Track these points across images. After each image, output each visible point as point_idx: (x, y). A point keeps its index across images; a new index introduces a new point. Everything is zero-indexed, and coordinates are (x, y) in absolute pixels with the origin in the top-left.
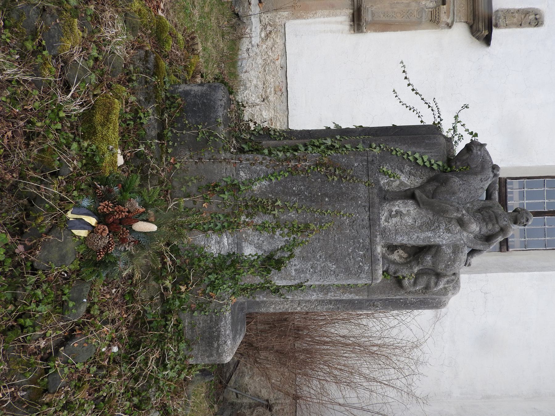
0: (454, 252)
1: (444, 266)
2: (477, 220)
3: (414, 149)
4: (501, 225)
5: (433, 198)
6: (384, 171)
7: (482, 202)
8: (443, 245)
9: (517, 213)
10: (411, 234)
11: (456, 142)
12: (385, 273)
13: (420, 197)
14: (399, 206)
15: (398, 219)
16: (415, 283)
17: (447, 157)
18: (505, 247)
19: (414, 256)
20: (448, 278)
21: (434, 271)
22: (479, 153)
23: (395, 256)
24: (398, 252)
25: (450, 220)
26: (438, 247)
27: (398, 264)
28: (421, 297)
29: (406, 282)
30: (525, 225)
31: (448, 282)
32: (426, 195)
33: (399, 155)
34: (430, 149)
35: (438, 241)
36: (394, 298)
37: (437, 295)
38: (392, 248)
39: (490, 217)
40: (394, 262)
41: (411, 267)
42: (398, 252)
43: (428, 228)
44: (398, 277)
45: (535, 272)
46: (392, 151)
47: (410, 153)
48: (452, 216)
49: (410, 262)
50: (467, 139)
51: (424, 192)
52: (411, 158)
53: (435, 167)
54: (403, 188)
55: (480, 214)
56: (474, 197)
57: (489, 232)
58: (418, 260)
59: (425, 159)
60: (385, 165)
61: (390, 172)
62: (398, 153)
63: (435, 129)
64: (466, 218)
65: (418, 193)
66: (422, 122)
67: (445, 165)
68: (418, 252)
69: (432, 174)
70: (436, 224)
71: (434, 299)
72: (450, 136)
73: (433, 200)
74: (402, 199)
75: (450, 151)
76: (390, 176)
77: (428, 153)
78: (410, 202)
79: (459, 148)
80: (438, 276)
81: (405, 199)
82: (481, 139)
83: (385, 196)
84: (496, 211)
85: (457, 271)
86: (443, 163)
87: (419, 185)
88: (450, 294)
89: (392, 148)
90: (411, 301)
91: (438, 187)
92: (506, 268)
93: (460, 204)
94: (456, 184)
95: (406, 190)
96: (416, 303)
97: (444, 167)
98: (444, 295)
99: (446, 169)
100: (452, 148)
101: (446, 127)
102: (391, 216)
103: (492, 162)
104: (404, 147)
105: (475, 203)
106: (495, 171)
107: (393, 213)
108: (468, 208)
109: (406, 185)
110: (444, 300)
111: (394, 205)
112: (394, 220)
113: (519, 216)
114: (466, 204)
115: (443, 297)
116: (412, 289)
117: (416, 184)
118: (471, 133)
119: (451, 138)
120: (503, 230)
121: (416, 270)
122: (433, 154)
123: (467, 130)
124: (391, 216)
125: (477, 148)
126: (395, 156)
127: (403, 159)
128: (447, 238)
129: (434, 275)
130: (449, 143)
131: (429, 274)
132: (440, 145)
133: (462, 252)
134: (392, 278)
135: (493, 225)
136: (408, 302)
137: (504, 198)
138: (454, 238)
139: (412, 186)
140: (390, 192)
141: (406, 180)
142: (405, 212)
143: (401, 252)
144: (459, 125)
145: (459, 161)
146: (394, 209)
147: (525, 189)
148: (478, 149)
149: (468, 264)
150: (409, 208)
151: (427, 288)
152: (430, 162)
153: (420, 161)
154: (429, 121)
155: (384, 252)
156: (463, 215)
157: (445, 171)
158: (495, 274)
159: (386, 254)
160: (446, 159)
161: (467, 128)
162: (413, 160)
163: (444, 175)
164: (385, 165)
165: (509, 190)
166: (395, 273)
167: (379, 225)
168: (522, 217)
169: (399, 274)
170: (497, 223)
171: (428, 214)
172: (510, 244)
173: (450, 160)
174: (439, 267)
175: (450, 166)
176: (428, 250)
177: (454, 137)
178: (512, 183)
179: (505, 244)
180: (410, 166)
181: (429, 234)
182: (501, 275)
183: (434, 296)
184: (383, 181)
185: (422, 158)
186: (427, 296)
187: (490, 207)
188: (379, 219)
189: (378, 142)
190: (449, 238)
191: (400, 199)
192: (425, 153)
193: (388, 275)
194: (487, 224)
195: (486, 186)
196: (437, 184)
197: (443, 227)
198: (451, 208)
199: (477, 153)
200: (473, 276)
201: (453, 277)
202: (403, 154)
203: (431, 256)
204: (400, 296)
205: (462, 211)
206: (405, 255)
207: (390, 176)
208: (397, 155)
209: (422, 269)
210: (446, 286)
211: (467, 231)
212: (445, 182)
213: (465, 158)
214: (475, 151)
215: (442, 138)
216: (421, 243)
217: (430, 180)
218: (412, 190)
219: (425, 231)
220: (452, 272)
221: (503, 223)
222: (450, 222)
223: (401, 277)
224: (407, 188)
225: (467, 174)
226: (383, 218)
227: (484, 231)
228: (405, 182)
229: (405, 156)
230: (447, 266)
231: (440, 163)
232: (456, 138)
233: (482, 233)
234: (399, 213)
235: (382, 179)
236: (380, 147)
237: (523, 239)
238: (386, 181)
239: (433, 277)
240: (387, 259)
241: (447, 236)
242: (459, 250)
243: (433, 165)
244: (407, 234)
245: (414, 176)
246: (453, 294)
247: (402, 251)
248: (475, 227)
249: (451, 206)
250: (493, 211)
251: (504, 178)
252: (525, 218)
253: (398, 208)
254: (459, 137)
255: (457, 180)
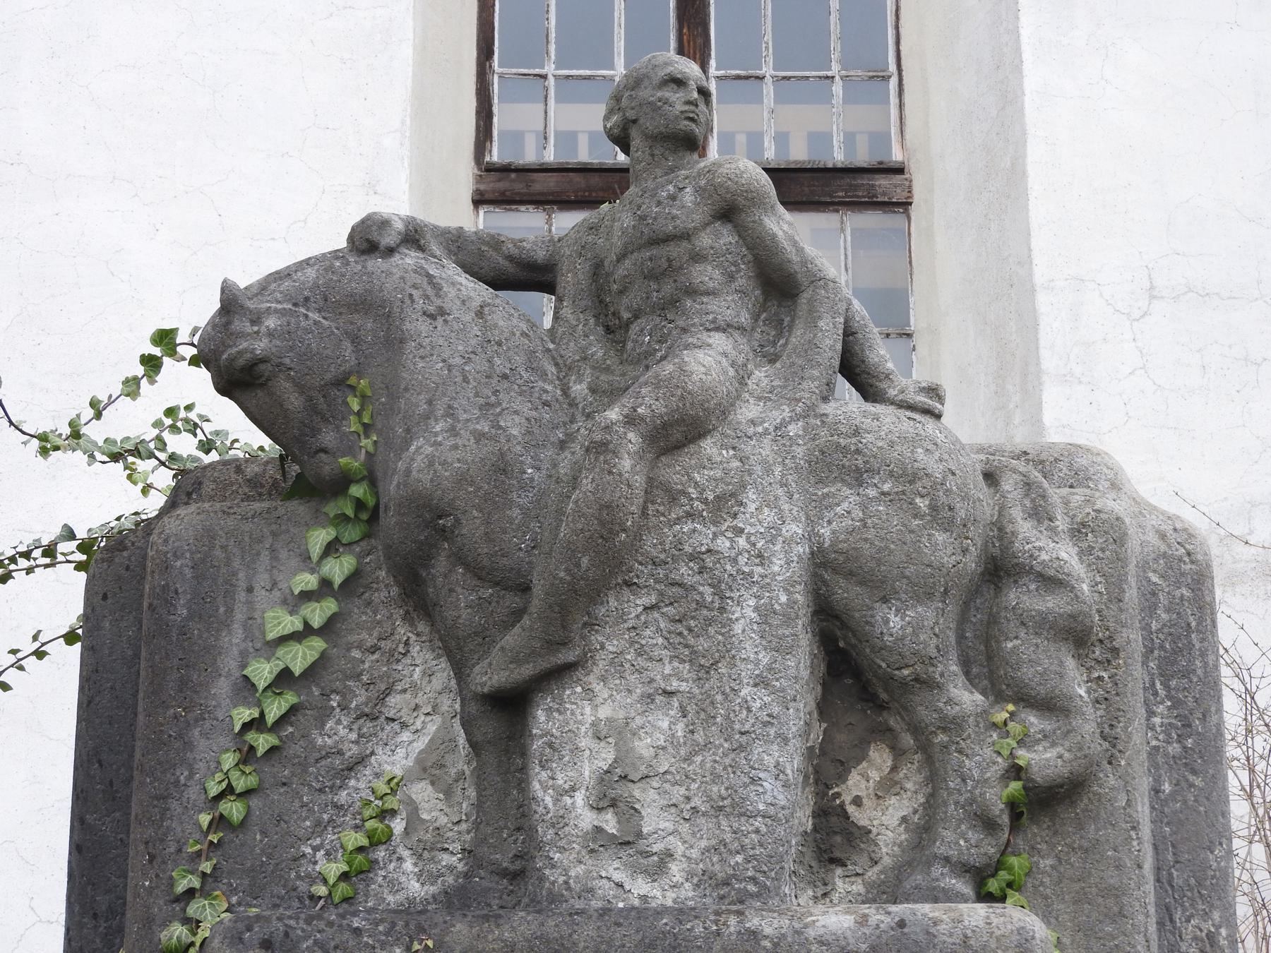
0: (858, 477)
1: (940, 537)
2: (668, 343)
3: (222, 688)
4: (698, 218)
5: (526, 589)
6: (345, 876)
7: (567, 312)
8: (812, 535)
9: (634, 132)
10: (744, 722)
11: (207, 447)
12: (993, 886)
13: (516, 660)
14: (565, 788)
15: (648, 799)
16: (1052, 706)
17: (289, 495)
18: (882, 182)
19: (881, 707)
20: (1016, 513)
21: (972, 594)
22: (271, 322)
23: (886, 819)
24: (857, 801)
25: (660, 493)
26: (825, 567)
27: (932, 805)
28: (1136, 672)
29: (1045, 760)
30: (704, 93)
31: (1040, 514)
32: (507, 625)
33: (252, 781)
34: (229, 594)
35: (785, 568)
36: (1146, 831)
37: (1122, 579)
38: (832, 840)
39: (654, 276)
40: (923, 831)
41: (953, 725)
42: (857, 801)
43: (709, 622)
44: (1012, 805)
45: (1025, 33)
46: (220, 822)
47: (244, 714)
48: (639, 481)
49: (916, 729)
50: (189, 384)
51: (485, 638)
52: (274, 710)
53: (338, 569)
54: (460, 761)
55: (635, 328)
56: (531, 354)
57: (741, 282)
58: (904, 684)
59: (291, 623)
60: (306, 868)
61: (354, 839)
62: (240, 784)
63: (117, 565)
64: (650, 404)
65: (492, 674)
66: (70, 638)
67: (332, 509)
68: (856, 684)
69: (385, 588)
70: (685, 572)
71: (1150, 597)
72: (164, 479)
73: (538, 590)
74: (523, 769)
75: (254, 482)
76: (376, 841)
77: (250, 604)
78: (542, 719)
79: (243, 434)
80: (1000, 569)
81: (524, 753)
82: (194, 313)
83: (504, 874)
84: (618, 242)
85: (975, 463)
86: (319, 520)
87: (444, 663)
88: (1110, 504)
89: (205, 819)
90: (1168, 728)
91: (459, 558)
92: (1004, 180)
93: (570, 437)
94: (452, 456)
95: (469, 741)
96: (1177, 704)
97: (343, 519)
98: (1120, 540)
99: (359, 504)
100: (238, 466)
101: (108, 499)
102: (628, 842)
103: (336, 254)
104: (202, 744)
105: (570, 352)
106: (388, 240)
107: (610, 823)
108: (593, 390)
109: (442, 744)
110: (1152, 538)
111: (559, 822)
112: (655, 821)
113: (649, 124)
114: (573, 404)
115: (1133, 545)
116: (1088, 724)
117: (438, 682)
118: (152, 364)
119: (181, 474)
120: (730, 210)
121: (966, 698)
122: (262, 579)
123: (131, 387)
124: (628, 842)
125: (242, 335)
126: (255, 802)
127: (277, 753)
128: (768, 515)
129: (998, 589)
130: (208, 487)
131: (993, 620)
132: (209, 535)
133: (857, 432)
134: (1020, 842)
135: (697, 257)
136: (1174, 749)
137: (595, 180)
138: (768, 471)
139: (451, 704)
140: (481, 841)
141: (411, 741)
142: (607, 756)
143: (857, 784)
144: (96, 432)
145: (315, 431)
146: (586, 819)
147: (550, 69)
148: (249, 329)
149: (928, 405)
150: (585, 728)
151: (1077, 635)
152: (307, 596)
153: (299, 658)
154: (61, 596)
155: (858, 887)
156: (631, 420)
157: (370, 515)
158: (1040, 242)
159: (872, 874)
160: (298, 508)
161: (117, 389)
162: (290, 698)
163: (389, 520)
164: (306, 868)
165: (550, 156)
166: (989, 825)
167: (681, 913)
168: (655, 108)
169: (996, 798)
170: (686, 236)
171: (622, 617)
172: (863, 158)
173: (303, 479)
174: (948, 561)
175: (341, 484)
176: (844, 626)
177: (173, 457)
178: (516, 138)
179: (863, 180)
180: (324, 714)
181: (744, 613)
182: (1040, 208)
183: (1132, 594)
184: (407, 880)
185: (283, 640)
186: (1132, 639)
187: (597, 269)
188: (643, 913)
189: (160, 906)
190: (773, 504)
191: (522, 784)
192: (253, 626)
193: (999, 865)
194: (692, 292)
195: (478, 291)
196: (441, 564)
197: (702, 535)
198: (586, 483)
199: (271, 334)
200: (1049, 361)
201: (1009, 484)
202: (247, 756)
203: (881, 611)
204: (1132, 792)
205: (608, 428)
206: (879, 759)
207: (376, 841)
208: (248, 793)
209: (966, 664)
210: (1062, 523)
211: (734, 399)
212: (433, 519)
213: (294, 401)
214: (261, 346)
215: (171, 525)
216: (800, 663)
217: (417, 598)
218: (473, 708)
219: (728, 636)
220: (981, 491)
221: (688, 206)
222: (673, 497)
223: (1015, 786)
224: (462, 739)
225: (393, 389)
226: (640, 887)
227: (731, 305)
228: (421, 744)
229: (263, 742)
230: (941, 516)
231: (319, 538)
232: (184, 445)
233: (744, 318)
234: (612, 792)
235: (394, 886)
236: (190, 893)
237: (838, 88)
238: (408, 865)
239: (1012, 596)
240: (901, 870)
241: (755, 514)
242: (845, 450)
243: (326, 583)
244: (741, 748)
245: (388, 692)
246: (1115, 486)
247: (854, 778)
248: (708, 360)
249: (575, 482)
250: (621, 257)
251: (479, 179)
252: (666, 93)
253: (579, 797)
254: (174, 429)
255: (421, 449)
